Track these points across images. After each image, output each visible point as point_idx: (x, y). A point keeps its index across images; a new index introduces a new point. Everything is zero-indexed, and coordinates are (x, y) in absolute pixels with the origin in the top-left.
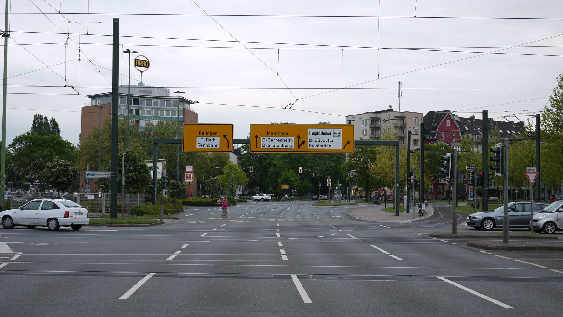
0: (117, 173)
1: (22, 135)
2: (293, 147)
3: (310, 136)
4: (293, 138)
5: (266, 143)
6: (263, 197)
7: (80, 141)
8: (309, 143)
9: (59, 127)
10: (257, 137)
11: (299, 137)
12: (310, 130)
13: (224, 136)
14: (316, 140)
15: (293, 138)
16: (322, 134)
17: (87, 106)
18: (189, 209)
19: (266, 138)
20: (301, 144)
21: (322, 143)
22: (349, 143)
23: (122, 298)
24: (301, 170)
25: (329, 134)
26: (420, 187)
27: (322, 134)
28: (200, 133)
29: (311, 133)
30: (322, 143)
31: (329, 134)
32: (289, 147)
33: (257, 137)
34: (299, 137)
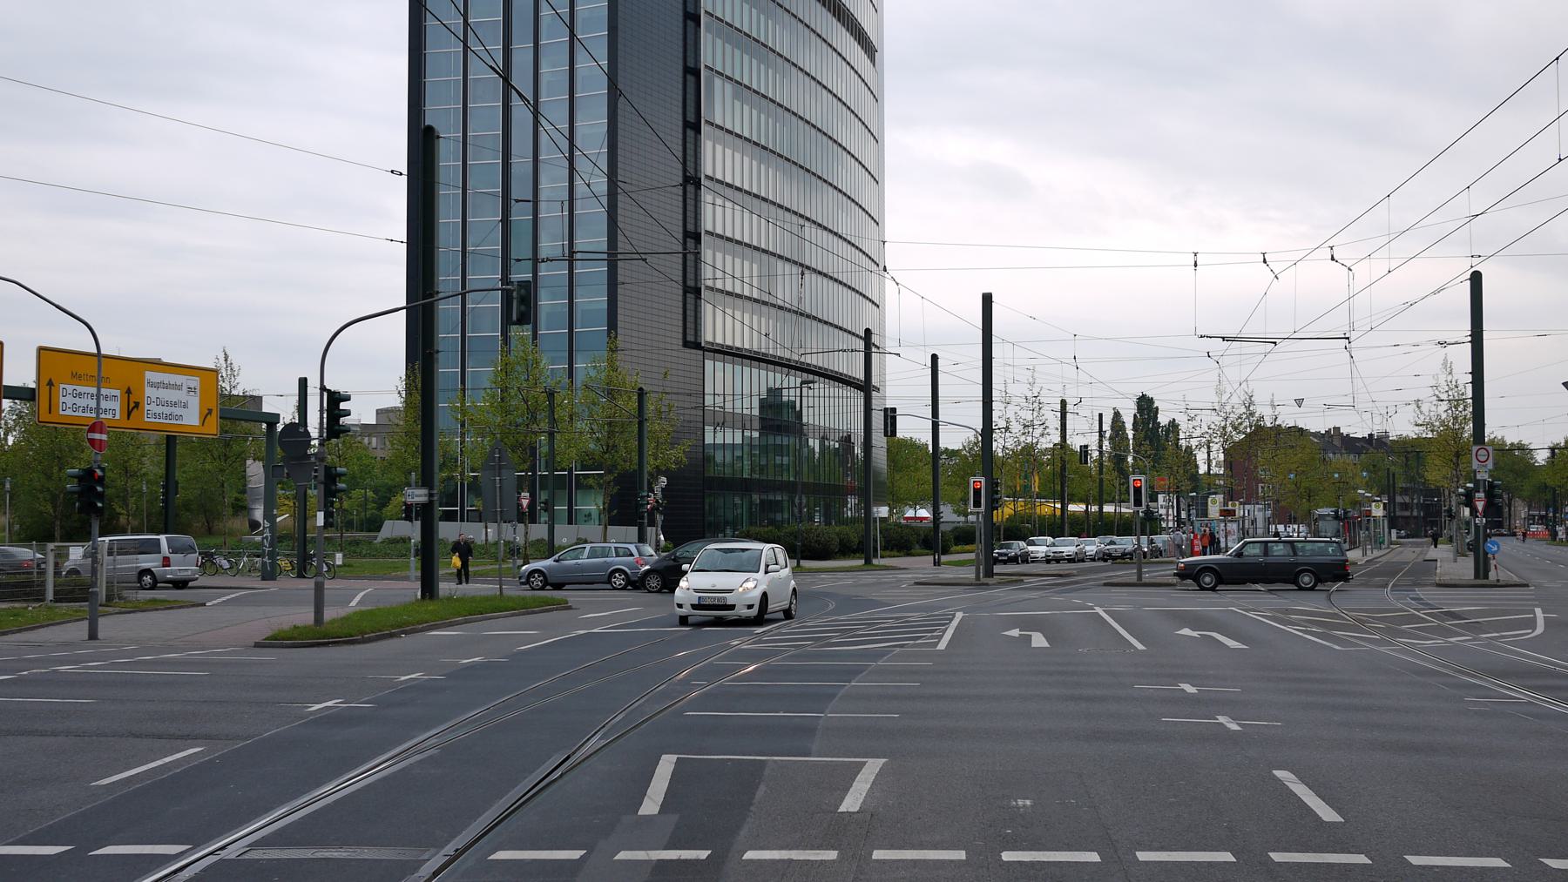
0: (1222, 482)
1: (1521, 447)
2: (117, 417)
3: (149, 391)
4: (117, 393)
5: (69, 400)
6: (149, 562)
7: (1083, 435)
8: (147, 407)
9: (1508, 442)
10: (50, 384)
11: (129, 391)
12: (151, 376)
13: (50, 380)
14: (160, 402)
15: (117, 393)
16: (167, 386)
17: (993, 387)
18: (1466, 556)
19: (70, 388)
20: (133, 408)
21: (167, 410)
22: (210, 411)
23: (1272, 855)
24: (977, 492)
25: (178, 387)
26: (1205, 554)
27: (167, 386)
28: (74, 375)
29: (152, 385)
30: (167, 410)
31: (178, 387)
32: (110, 416)
33: (50, 384)
34: (129, 391)
